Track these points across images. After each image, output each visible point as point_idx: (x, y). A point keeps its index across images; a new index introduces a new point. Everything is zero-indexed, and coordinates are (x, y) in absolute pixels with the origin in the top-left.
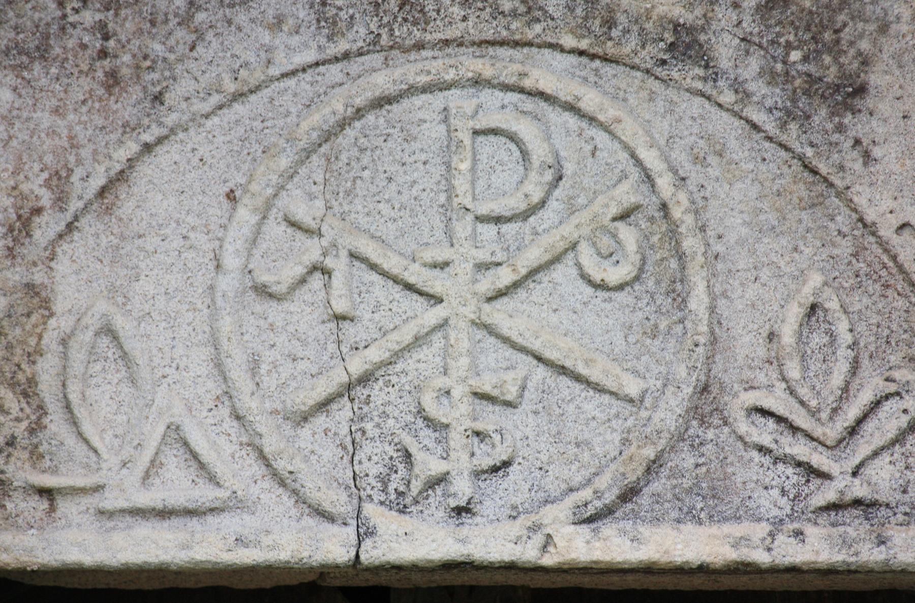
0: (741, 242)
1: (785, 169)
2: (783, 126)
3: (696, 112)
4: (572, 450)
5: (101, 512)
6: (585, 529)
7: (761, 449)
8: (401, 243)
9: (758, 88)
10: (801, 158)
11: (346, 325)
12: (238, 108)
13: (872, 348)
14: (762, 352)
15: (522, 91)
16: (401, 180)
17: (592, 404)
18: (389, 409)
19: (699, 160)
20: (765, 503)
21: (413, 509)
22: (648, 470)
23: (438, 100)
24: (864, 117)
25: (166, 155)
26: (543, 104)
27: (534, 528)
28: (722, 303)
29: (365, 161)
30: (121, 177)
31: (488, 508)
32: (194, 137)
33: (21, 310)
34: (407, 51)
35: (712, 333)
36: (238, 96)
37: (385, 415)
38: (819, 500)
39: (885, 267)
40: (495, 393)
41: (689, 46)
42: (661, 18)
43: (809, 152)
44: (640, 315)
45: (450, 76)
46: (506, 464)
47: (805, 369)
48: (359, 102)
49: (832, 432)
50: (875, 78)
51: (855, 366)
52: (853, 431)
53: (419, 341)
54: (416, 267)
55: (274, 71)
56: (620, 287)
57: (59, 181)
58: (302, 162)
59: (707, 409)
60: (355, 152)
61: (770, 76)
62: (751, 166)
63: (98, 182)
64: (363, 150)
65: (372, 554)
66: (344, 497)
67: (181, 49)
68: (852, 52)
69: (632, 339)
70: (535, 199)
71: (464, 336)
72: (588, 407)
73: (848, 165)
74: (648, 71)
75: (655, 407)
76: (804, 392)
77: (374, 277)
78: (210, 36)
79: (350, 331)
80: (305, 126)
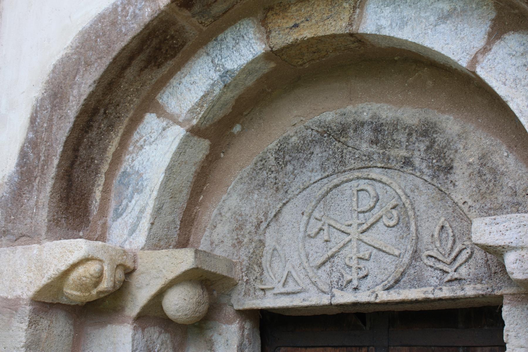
0: (424, 211)
1: (434, 191)
2: (432, 179)
3: (411, 179)
4: (383, 271)
5: (274, 294)
6: (386, 292)
7: (431, 267)
8: (341, 221)
9: (426, 170)
10: (438, 187)
11: (328, 243)
12: (304, 192)
13: (459, 236)
14: (430, 240)
15: (369, 179)
16: (341, 205)
17: (388, 258)
18: (339, 264)
19: (412, 191)
20: (432, 281)
21: (345, 289)
22: (402, 274)
23: (349, 184)
24: (453, 175)
25: (289, 205)
26: (374, 182)
27: (373, 292)
28: (420, 228)
29: (333, 201)
30: (279, 212)
31: (363, 288)
32: (295, 200)
33: (258, 246)
34: (342, 173)
35: (417, 236)
36: (304, 189)
37: (338, 265)
38: (446, 279)
39: (461, 214)
40: (363, 257)
41: (408, 162)
42: (401, 156)
43: (439, 185)
44: (399, 233)
45: (351, 177)
46: (366, 276)
47: (441, 244)
48: (330, 187)
49: (449, 260)
50: (455, 164)
51: (454, 242)
52: (455, 259)
53: (345, 245)
54: (344, 226)
55: (312, 182)
56: (393, 226)
57: (266, 214)
58: (318, 203)
59: (417, 257)
60: (330, 199)
61: (428, 167)
62: (425, 191)
63: (274, 213)
64: (332, 199)
65: (335, 301)
66: (328, 287)
67: (291, 180)
68: (449, 158)
69: (397, 240)
70: (372, 206)
71: (355, 243)
72: (386, 259)
73: (449, 188)
74: (399, 170)
75: (403, 258)
76: (440, 250)
77: (335, 230)
78: (298, 176)
79: (329, 244)
80: (318, 194)
